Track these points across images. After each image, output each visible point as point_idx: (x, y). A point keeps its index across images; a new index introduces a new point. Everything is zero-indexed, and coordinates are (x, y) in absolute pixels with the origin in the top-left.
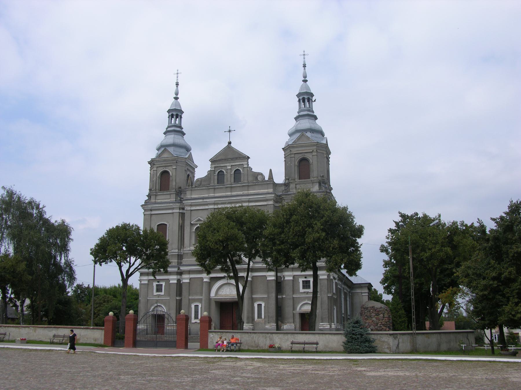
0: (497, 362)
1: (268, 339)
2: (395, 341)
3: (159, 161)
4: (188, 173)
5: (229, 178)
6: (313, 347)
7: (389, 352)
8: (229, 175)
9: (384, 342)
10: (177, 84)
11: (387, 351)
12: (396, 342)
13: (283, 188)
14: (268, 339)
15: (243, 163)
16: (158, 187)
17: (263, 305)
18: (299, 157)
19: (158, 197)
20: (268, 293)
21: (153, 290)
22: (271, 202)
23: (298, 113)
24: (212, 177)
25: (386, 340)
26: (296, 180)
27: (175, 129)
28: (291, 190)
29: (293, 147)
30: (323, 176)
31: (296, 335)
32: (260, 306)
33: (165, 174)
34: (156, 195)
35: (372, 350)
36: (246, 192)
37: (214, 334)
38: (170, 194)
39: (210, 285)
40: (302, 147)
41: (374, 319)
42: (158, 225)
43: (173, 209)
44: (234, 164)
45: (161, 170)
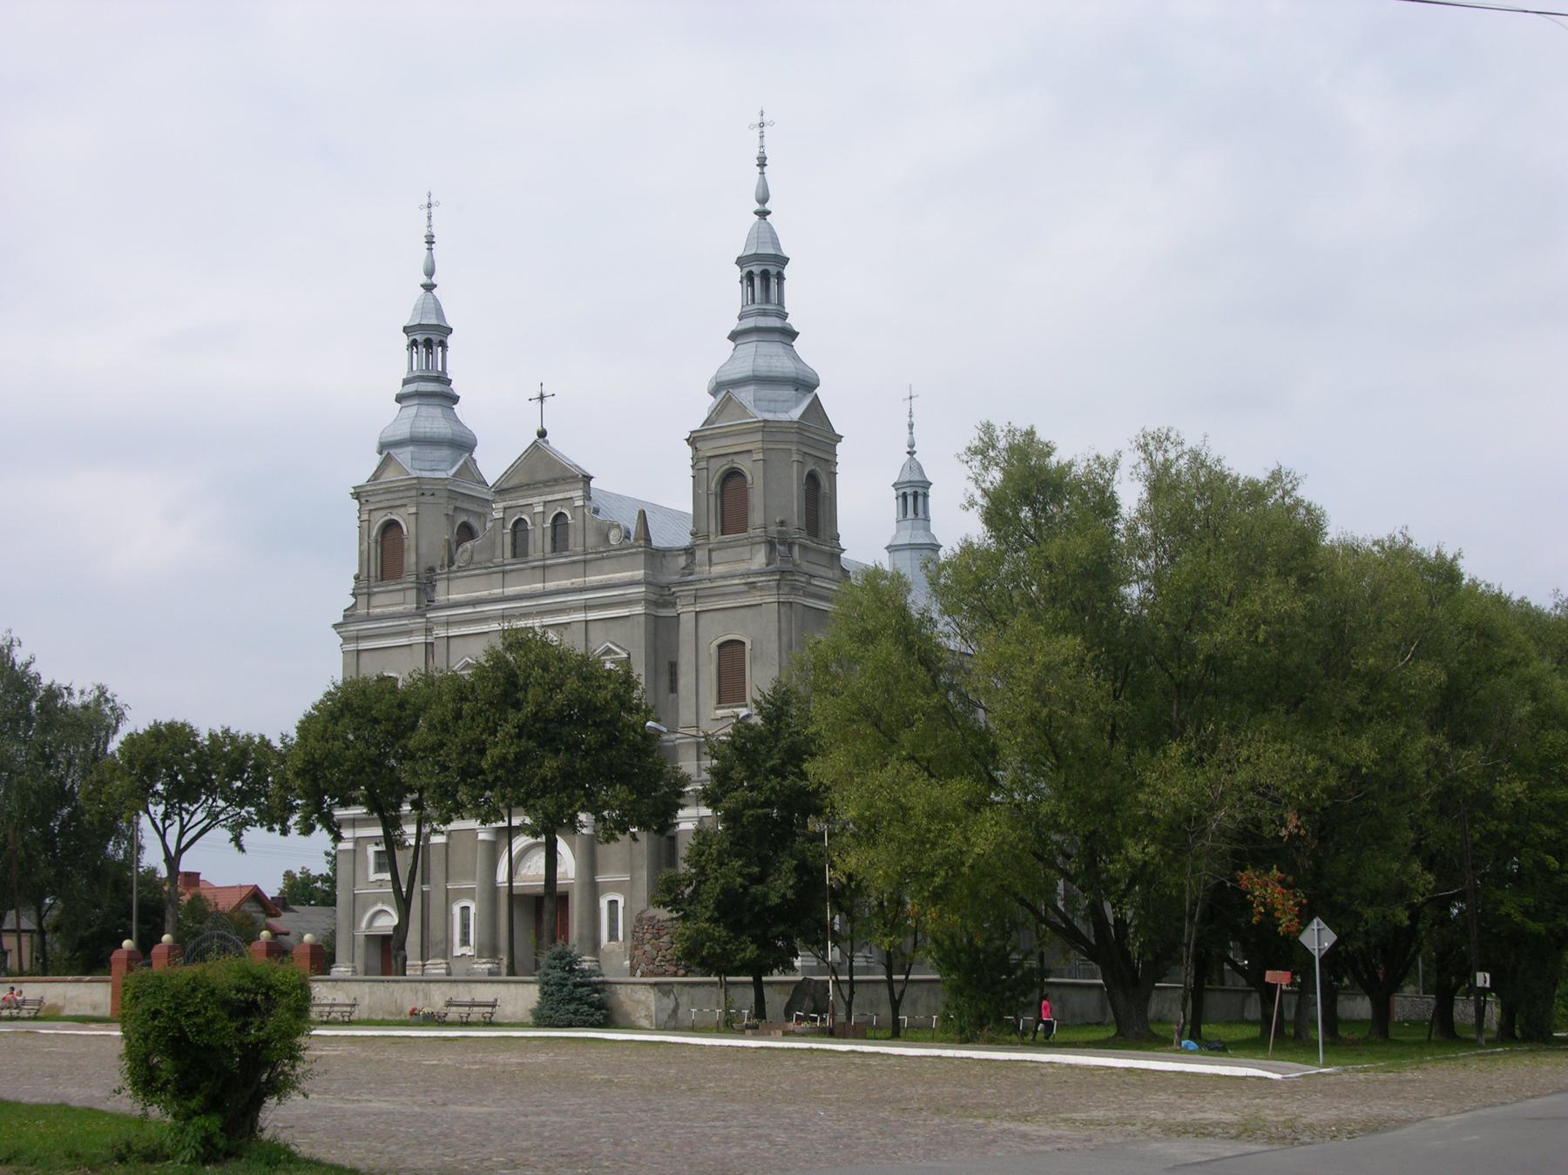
1: (420, 994)
2: (665, 1000)
3: (374, 493)
4: (463, 518)
5: (539, 539)
6: (477, 1014)
8: (539, 532)
9: (639, 1002)
10: (430, 241)
11: (645, 1023)
12: (669, 1003)
13: (682, 561)
14: (420, 994)
15: (530, 501)
17: (473, 910)
19: (375, 600)
20: (632, 870)
21: (366, 868)
23: (741, 318)
24: (499, 539)
26: (712, 537)
27: (432, 389)
29: (704, 438)
30: (782, 523)
32: (613, 903)
33: (391, 526)
34: (369, 595)
35: (607, 1023)
36: (578, 581)
38: (404, 590)
39: (493, 850)
41: (647, 947)
42: (720, 646)
43: (409, 633)
44: (550, 498)
45: (380, 519)
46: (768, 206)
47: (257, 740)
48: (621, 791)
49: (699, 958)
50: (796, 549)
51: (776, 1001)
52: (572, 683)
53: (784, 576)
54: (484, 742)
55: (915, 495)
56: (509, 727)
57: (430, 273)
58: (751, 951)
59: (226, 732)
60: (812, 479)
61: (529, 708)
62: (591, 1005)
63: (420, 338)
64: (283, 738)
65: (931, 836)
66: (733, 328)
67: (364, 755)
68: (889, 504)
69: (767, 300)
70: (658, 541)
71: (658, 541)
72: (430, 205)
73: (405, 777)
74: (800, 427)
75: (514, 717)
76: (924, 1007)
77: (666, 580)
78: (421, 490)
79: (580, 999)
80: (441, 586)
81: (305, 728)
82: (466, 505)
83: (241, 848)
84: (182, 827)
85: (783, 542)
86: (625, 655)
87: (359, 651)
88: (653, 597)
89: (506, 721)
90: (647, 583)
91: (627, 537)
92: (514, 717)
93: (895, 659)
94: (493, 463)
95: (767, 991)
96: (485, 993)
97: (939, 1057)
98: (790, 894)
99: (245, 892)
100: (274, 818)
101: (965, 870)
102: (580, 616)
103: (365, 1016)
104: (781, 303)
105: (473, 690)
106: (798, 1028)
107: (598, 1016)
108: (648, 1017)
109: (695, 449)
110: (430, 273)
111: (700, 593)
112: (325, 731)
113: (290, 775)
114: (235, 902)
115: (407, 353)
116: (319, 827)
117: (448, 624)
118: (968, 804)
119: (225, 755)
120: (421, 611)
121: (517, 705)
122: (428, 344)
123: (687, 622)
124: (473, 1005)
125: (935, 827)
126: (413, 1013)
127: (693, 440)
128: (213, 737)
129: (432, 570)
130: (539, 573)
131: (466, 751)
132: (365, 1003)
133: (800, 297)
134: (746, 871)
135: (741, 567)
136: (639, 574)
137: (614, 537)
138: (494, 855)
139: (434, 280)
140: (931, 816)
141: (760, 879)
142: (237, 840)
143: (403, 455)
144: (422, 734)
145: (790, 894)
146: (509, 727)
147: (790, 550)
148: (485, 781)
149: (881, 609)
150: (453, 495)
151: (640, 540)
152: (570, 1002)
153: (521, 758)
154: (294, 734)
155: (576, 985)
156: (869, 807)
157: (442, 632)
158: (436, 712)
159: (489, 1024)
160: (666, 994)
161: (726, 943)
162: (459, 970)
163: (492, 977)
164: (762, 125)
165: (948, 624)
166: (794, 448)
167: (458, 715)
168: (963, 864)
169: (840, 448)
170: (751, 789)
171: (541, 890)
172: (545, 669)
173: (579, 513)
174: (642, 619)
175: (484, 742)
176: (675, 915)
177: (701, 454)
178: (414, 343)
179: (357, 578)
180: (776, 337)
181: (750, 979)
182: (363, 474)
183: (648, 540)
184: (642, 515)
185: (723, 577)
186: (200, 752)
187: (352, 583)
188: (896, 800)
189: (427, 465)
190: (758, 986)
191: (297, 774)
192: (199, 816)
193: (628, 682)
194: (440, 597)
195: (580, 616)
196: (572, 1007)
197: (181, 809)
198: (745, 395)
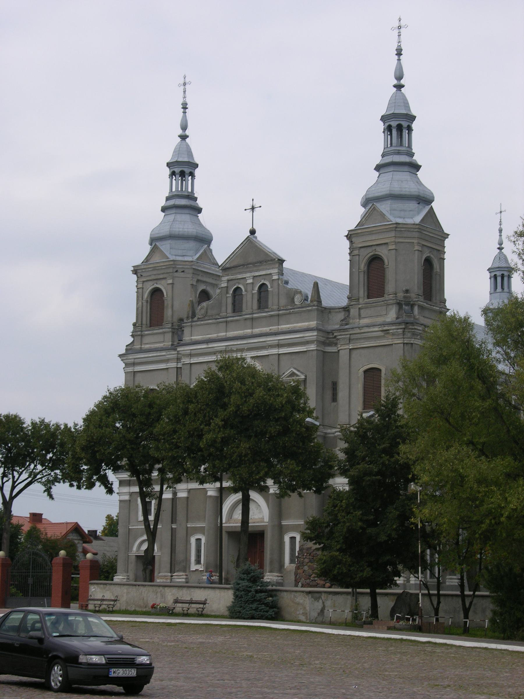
0: (312, 632)
1: (159, 595)
2: (316, 603)
4: (202, 287)
5: (250, 300)
6: (194, 608)
7: (304, 620)
8: (249, 296)
9: (298, 604)
10: (185, 107)
11: (303, 618)
12: (319, 605)
13: (341, 316)
15: (244, 276)
16: (146, 320)
18: (367, 254)
19: (146, 340)
22: (313, 347)
23: (383, 156)
25: (301, 601)
26: (361, 301)
28: (351, 321)
30: (407, 291)
31: (192, 590)
33: (156, 292)
34: (142, 336)
35: (277, 617)
36: (274, 328)
37: (96, 586)
38: (164, 333)
40: (371, 233)
41: (306, 568)
42: (365, 372)
43: (167, 361)
44: (257, 274)
45: (149, 287)
46: (402, 82)
47: (62, 427)
48: (292, 464)
49: (333, 574)
50: (416, 309)
51: (385, 605)
52: (260, 392)
53: (407, 325)
54: (202, 430)
55: (503, 276)
56: (218, 421)
57: (184, 127)
58: (367, 572)
59: (42, 422)
60: (428, 262)
61: (232, 408)
62: (267, 605)
63: (177, 170)
64: (76, 425)
65: (480, 495)
66: (378, 162)
67: (125, 437)
68: (485, 283)
69: (401, 145)
70: (326, 303)
71: (326, 303)
72: (185, 84)
73: (152, 452)
74: (420, 228)
75: (222, 414)
76: (484, 612)
77: (331, 326)
78: (174, 268)
79: (260, 601)
80: (187, 331)
81: (88, 420)
82: (205, 279)
83: (51, 496)
84: (14, 482)
85: (407, 304)
86: (303, 377)
87: (135, 372)
88: (322, 339)
89: (216, 416)
90: (318, 329)
91: (306, 299)
92: (222, 414)
93: (461, 375)
94: (222, 251)
95: (379, 600)
96: (199, 595)
97: (486, 649)
98: (394, 535)
99: (70, 527)
100: (74, 477)
101: (503, 519)
102: (275, 351)
103: (123, 608)
104: (410, 146)
105: (196, 397)
106: (397, 625)
107: (271, 612)
108: (305, 614)
109: (351, 242)
110: (184, 127)
111: (353, 337)
112: (101, 421)
113: (78, 450)
114: (64, 532)
115: (168, 180)
116: (98, 484)
117: (191, 355)
118: (508, 475)
119: (42, 436)
120: (174, 347)
121: (224, 406)
122: (182, 174)
123: (344, 356)
124: (191, 602)
125: (482, 489)
126: (153, 606)
127: (350, 236)
128: (34, 424)
129: (181, 320)
130: (249, 323)
131: (191, 436)
132: (123, 599)
133: (422, 143)
134: (365, 518)
135: (380, 320)
136: (313, 324)
137: (297, 300)
138: (206, 505)
139: (187, 132)
140: (480, 482)
141: (373, 524)
142: (48, 491)
143: (165, 246)
144: (164, 424)
145: (394, 535)
146: (218, 421)
147: (412, 309)
148: (203, 456)
149: (452, 342)
150: (196, 272)
151: (314, 301)
152: (252, 602)
153: (225, 441)
154: (81, 423)
155: (257, 592)
156: (439, 474)
157: (187, 361)
158: (171, 409)
159: (201, 615)
160: (317, 599)
161: (350, 566)
162: (193, 579)
163: (211, 584)
164: (400, 27)
165: (498, 352)
166: (415, 241)
167: (186, 412)
168: (502, 515)
169: (447, 242)
170: (371, 462)
171: (239, 529)
172: (243, 382)
173: (275, 284)
174: (315, 352)
175: (202, 430)
176: (318, 546)
177: (355, 245)
178: (173, 174)
179: (134, 325)
180: (406, 168)
181: (368, 591)
182: (139, 260)
183: (319, 301)
184: (316, 286)
185: (368, 326)
186: (26, 435)
187: (131, 328)
188: (456, 470)
189: (180, 252)
190: (374, 596)
191: (83, 449)
192: (25, 476)
193: (297, 392)
194: (187, 338)
195: (275, 351)
196: (254, 606)
197: (13, 470)
198: (384, 207)
